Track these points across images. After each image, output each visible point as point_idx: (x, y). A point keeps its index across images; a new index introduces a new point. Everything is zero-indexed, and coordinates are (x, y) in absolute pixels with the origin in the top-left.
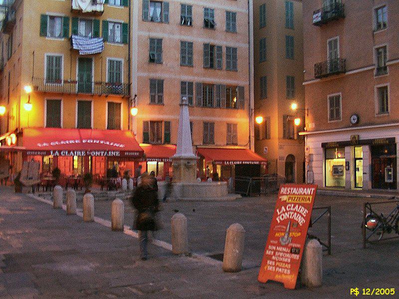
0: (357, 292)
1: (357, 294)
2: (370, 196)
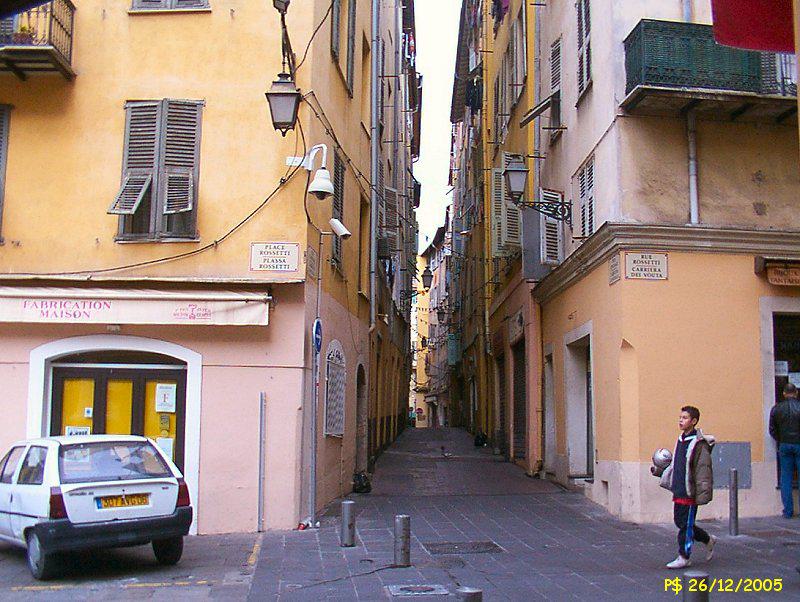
0: (677, 585)
1: (677, 590)
2: (403, 75)
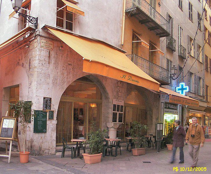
0: (177, 169)
1: (177, 171)
